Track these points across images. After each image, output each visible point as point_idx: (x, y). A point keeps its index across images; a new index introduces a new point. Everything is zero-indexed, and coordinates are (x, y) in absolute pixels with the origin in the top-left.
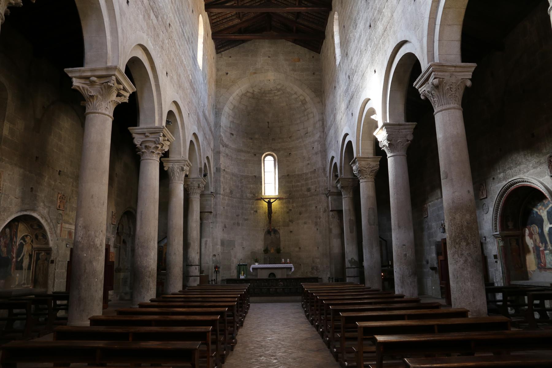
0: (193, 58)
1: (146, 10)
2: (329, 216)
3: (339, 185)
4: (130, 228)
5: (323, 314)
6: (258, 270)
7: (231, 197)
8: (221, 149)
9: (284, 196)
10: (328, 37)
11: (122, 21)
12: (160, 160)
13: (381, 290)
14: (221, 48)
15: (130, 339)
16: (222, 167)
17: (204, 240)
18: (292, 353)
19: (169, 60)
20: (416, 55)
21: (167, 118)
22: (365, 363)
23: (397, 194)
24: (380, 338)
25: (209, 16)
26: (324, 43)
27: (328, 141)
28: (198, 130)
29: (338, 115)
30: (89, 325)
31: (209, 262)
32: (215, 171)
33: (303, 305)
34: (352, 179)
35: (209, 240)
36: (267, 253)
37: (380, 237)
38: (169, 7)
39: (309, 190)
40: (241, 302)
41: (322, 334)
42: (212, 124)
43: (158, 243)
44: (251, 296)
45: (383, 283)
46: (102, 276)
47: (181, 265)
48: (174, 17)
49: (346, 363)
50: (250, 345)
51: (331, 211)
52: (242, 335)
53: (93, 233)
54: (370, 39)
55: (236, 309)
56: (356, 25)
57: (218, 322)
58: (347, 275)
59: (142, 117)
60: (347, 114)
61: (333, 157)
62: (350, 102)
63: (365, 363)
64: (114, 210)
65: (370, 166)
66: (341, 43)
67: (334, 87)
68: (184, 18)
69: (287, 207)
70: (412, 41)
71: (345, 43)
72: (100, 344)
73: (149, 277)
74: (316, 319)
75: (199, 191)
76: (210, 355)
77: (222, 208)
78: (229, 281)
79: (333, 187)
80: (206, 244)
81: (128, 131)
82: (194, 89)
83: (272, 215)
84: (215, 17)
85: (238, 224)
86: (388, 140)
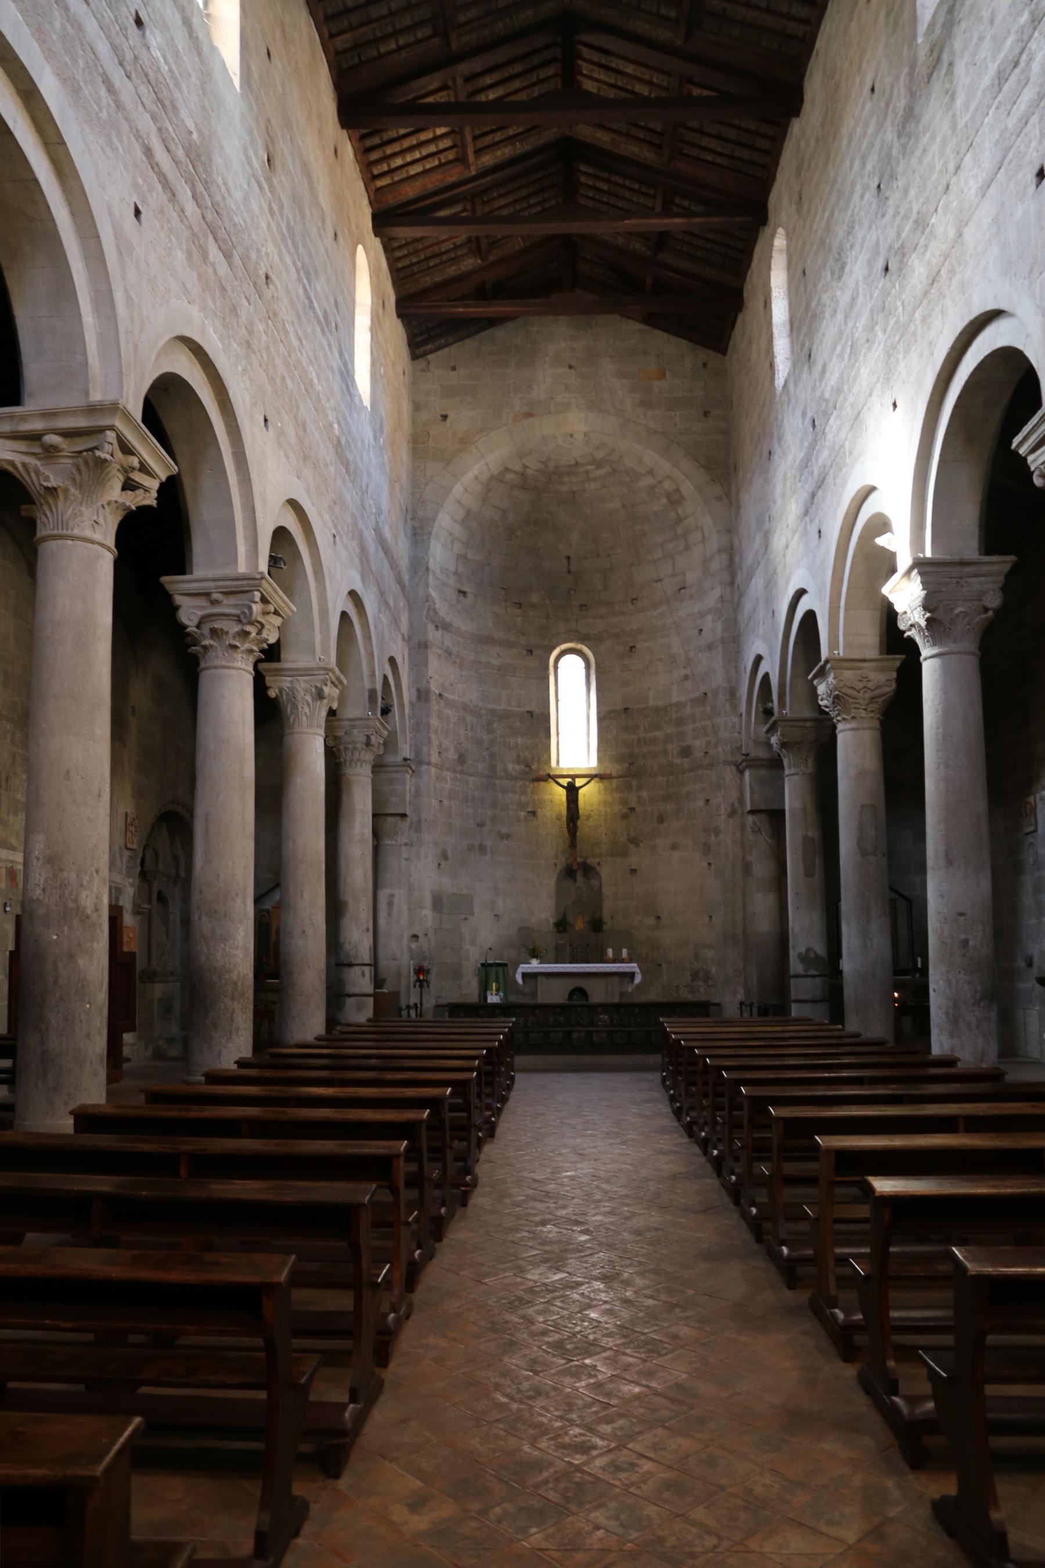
0: (341, 373)
1: (194, 235)
2: (743, 826)
3: (774, 740)
4: (176, 858)
5: (721, 1108)
6: (540, 979)
7: (462, 772)
8: (430, 637)
9: (614, 769)
10: (753, 304)
11: (123, 269)
12: (255, 668)
13: (891, 1043)
14: (425, 342)
15: (183, 1171)
16: (435, 689)
17: (383, 894)
18: (633, 1215)
19: (272, 380)
20: (1028, 354)
21: (271, 550)
22: (838, 1251)
23: (947, 766)
24: (883, 1185)
25: (387, 249)
26: (738, 323)
27: (746, 612)
28: (363, 581)
29: (776, 536)
30: (71, 1131)
31: (398, 954)
32: (414, 699)
33: (664, 1079)
34: (814, 720)
35: (400, 895)
36: (565, 930)
37: (891, 889)
38: (264, 225)
39: (686, 752)
40: (489, 1068)
41: (718, 1165)
42: (404, 563)
43: (257, 900)
44: (520, 1051)
45: (897, 1020)
46: (102, 996)
47: (322, 965)
48: (280, 253)
49: (785, 1250)
50: (513, 1191)
51: (752, 812)
52: (494, 1161)
53: (73, 875)
54: (884, 308)
55: (474, 1089)
56: (843, 268)
57: (424, 1127)
58: (793, 996)
59: (198, 547)
60: (805, 533)
61: (759, 659)
62: (813, 495)
63: (838, 1251)
64: (130, 810)
65: (870, 685)
66: (791, 322)
67: (765, 454)
68: (310, 256)
69: (623, 802)
70: (1018, 311)
71: (804, 323)
72: (103, 1184)
73: (233, 999)
74: (701, 1121)
75: (368, 756)
76: (403, 1219)
77: (435, 803)
78: (457, 1009)
79: (757, 743)
80: (390, 904)
81: (162, 587)
82: (346, 464)
83: (579, 823)
84: (405, 252)
85: (482, 849)
86: (926, 607)
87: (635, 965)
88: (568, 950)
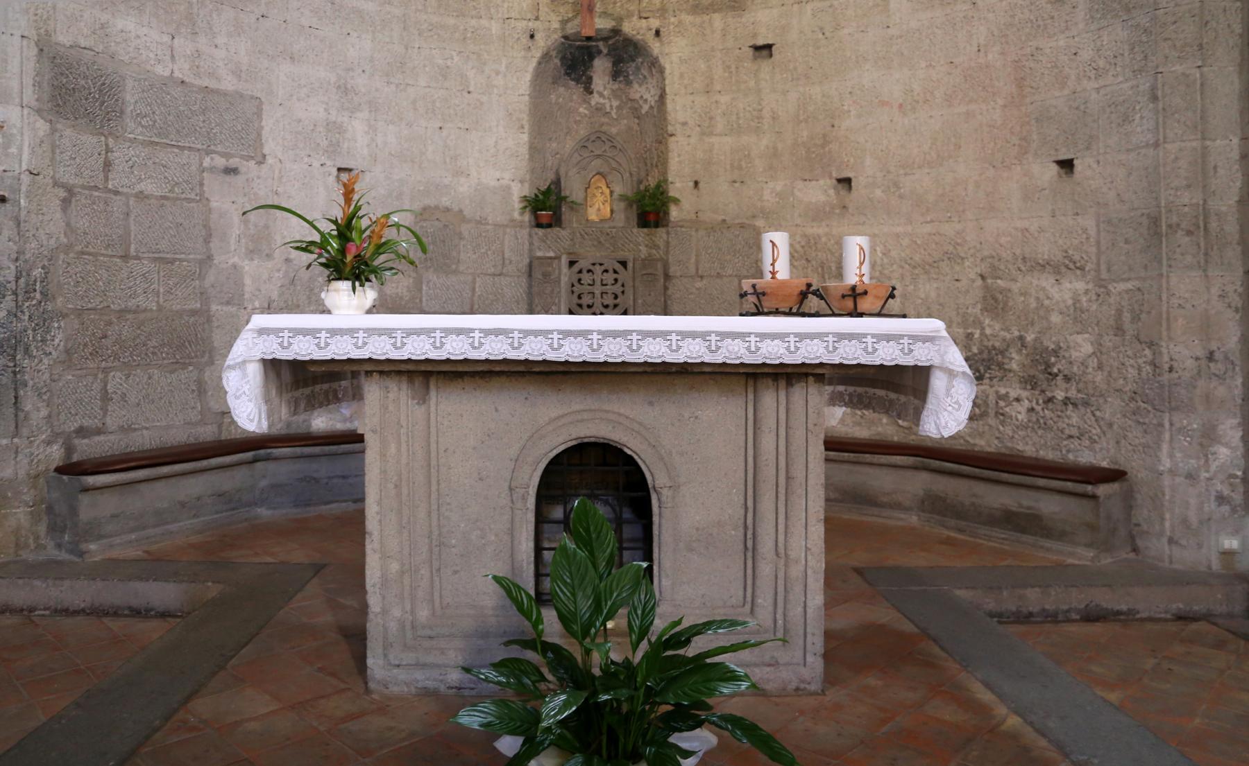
6: (373, 391)
36: (555, 221)
87: (935, 325)
88: (566, 275)
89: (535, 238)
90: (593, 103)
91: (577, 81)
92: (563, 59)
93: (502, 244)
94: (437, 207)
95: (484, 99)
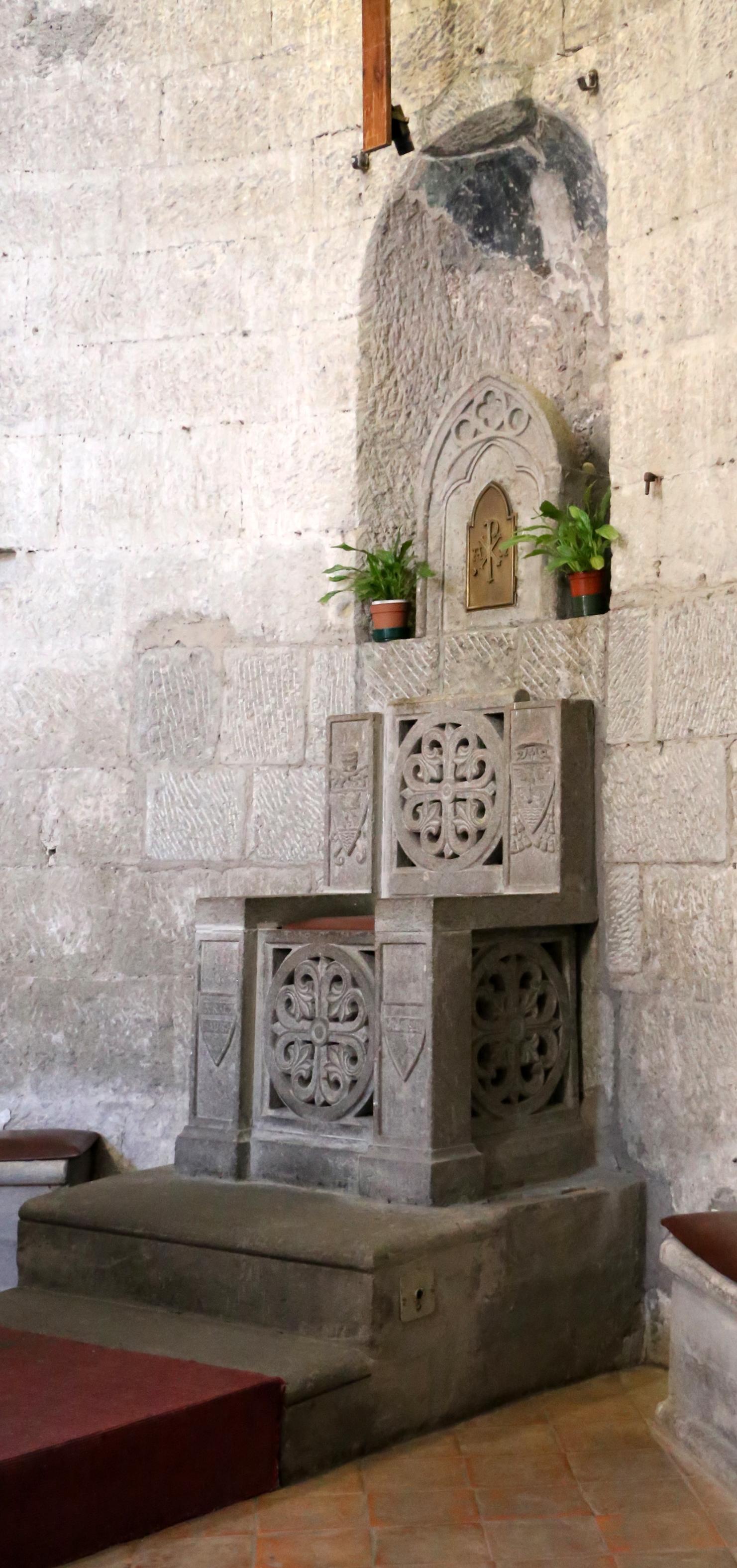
89: (368, 666)
90: (555, 296)
91: (511, 247)
92: (455, 202)
93: (304, 687)
94: (178, 615)
95: (274, 342)
